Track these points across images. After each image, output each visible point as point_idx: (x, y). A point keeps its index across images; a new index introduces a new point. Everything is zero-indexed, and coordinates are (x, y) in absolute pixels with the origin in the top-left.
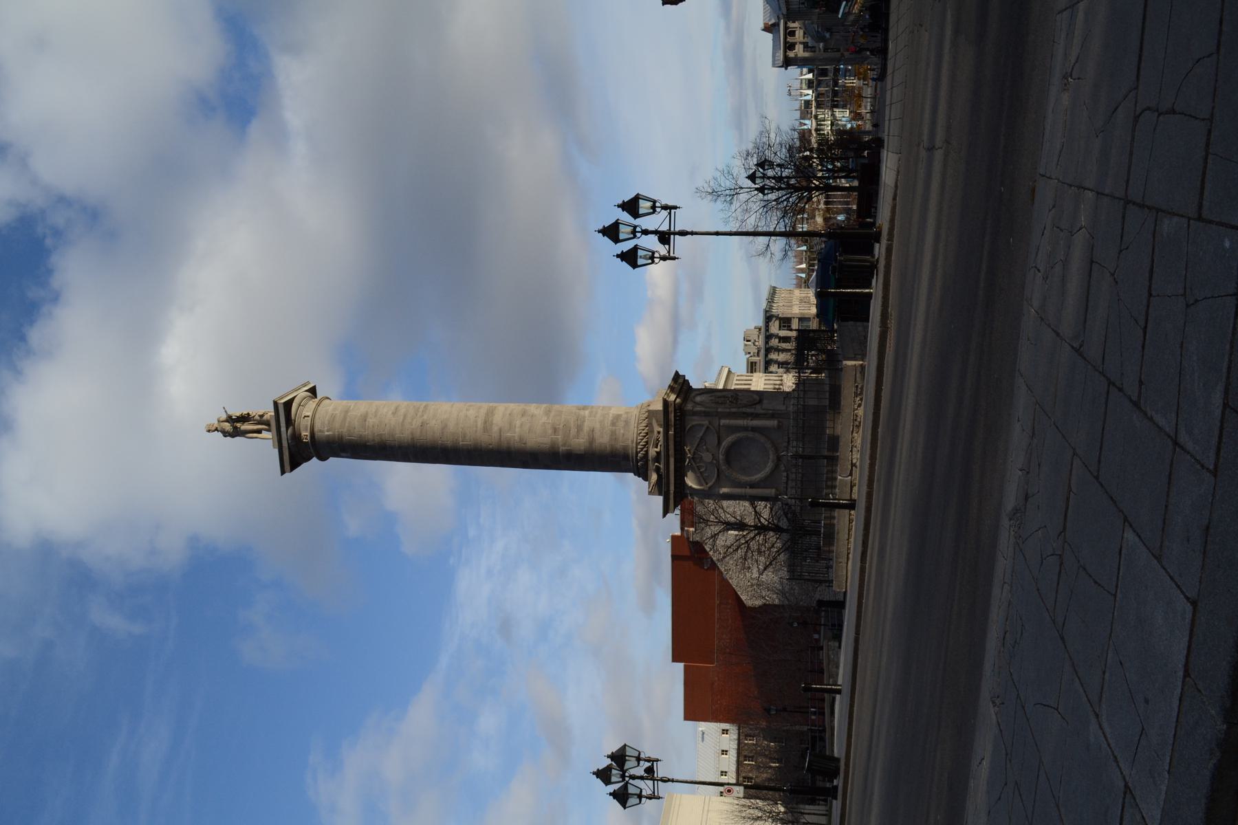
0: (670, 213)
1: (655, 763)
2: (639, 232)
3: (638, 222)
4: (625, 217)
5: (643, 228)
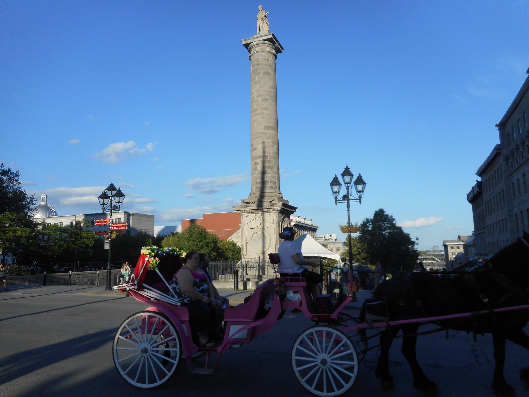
1: (358, 201)
3: (352, 184)
4: (355, 178)
5: (362, 196)
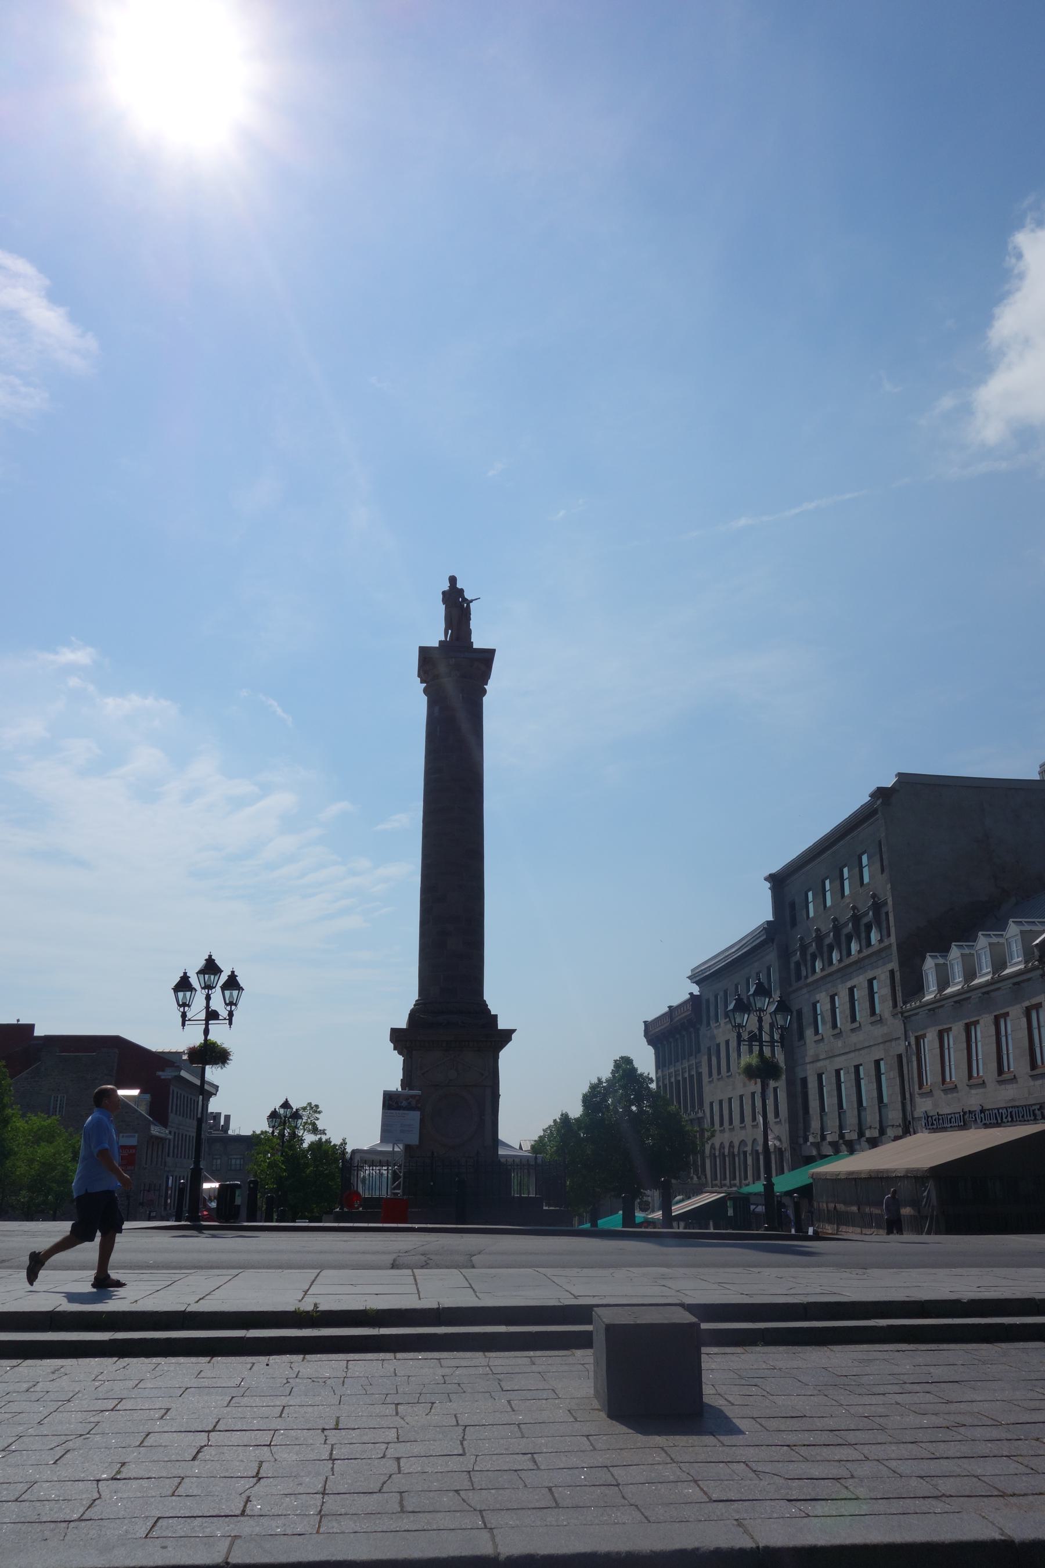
0: (225, 1019)
2: (231, 1008)
3: (218, 989)
4: (224, 978)
5: (234, 1012)
